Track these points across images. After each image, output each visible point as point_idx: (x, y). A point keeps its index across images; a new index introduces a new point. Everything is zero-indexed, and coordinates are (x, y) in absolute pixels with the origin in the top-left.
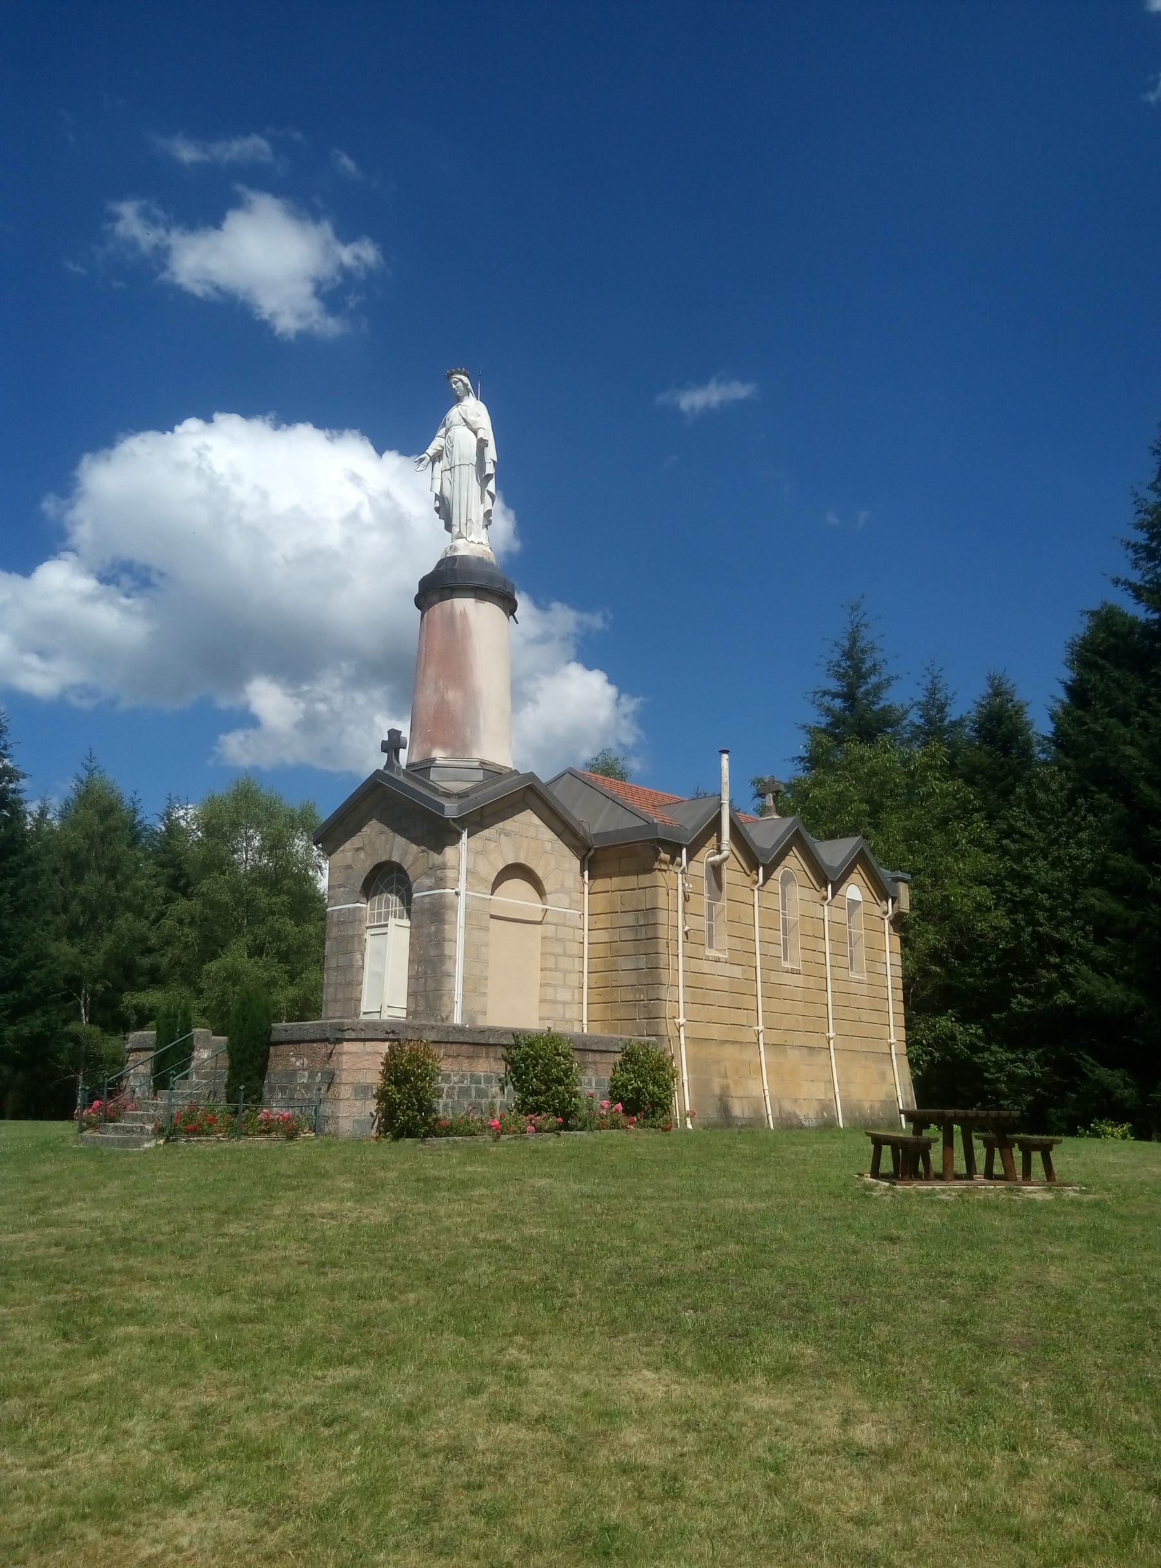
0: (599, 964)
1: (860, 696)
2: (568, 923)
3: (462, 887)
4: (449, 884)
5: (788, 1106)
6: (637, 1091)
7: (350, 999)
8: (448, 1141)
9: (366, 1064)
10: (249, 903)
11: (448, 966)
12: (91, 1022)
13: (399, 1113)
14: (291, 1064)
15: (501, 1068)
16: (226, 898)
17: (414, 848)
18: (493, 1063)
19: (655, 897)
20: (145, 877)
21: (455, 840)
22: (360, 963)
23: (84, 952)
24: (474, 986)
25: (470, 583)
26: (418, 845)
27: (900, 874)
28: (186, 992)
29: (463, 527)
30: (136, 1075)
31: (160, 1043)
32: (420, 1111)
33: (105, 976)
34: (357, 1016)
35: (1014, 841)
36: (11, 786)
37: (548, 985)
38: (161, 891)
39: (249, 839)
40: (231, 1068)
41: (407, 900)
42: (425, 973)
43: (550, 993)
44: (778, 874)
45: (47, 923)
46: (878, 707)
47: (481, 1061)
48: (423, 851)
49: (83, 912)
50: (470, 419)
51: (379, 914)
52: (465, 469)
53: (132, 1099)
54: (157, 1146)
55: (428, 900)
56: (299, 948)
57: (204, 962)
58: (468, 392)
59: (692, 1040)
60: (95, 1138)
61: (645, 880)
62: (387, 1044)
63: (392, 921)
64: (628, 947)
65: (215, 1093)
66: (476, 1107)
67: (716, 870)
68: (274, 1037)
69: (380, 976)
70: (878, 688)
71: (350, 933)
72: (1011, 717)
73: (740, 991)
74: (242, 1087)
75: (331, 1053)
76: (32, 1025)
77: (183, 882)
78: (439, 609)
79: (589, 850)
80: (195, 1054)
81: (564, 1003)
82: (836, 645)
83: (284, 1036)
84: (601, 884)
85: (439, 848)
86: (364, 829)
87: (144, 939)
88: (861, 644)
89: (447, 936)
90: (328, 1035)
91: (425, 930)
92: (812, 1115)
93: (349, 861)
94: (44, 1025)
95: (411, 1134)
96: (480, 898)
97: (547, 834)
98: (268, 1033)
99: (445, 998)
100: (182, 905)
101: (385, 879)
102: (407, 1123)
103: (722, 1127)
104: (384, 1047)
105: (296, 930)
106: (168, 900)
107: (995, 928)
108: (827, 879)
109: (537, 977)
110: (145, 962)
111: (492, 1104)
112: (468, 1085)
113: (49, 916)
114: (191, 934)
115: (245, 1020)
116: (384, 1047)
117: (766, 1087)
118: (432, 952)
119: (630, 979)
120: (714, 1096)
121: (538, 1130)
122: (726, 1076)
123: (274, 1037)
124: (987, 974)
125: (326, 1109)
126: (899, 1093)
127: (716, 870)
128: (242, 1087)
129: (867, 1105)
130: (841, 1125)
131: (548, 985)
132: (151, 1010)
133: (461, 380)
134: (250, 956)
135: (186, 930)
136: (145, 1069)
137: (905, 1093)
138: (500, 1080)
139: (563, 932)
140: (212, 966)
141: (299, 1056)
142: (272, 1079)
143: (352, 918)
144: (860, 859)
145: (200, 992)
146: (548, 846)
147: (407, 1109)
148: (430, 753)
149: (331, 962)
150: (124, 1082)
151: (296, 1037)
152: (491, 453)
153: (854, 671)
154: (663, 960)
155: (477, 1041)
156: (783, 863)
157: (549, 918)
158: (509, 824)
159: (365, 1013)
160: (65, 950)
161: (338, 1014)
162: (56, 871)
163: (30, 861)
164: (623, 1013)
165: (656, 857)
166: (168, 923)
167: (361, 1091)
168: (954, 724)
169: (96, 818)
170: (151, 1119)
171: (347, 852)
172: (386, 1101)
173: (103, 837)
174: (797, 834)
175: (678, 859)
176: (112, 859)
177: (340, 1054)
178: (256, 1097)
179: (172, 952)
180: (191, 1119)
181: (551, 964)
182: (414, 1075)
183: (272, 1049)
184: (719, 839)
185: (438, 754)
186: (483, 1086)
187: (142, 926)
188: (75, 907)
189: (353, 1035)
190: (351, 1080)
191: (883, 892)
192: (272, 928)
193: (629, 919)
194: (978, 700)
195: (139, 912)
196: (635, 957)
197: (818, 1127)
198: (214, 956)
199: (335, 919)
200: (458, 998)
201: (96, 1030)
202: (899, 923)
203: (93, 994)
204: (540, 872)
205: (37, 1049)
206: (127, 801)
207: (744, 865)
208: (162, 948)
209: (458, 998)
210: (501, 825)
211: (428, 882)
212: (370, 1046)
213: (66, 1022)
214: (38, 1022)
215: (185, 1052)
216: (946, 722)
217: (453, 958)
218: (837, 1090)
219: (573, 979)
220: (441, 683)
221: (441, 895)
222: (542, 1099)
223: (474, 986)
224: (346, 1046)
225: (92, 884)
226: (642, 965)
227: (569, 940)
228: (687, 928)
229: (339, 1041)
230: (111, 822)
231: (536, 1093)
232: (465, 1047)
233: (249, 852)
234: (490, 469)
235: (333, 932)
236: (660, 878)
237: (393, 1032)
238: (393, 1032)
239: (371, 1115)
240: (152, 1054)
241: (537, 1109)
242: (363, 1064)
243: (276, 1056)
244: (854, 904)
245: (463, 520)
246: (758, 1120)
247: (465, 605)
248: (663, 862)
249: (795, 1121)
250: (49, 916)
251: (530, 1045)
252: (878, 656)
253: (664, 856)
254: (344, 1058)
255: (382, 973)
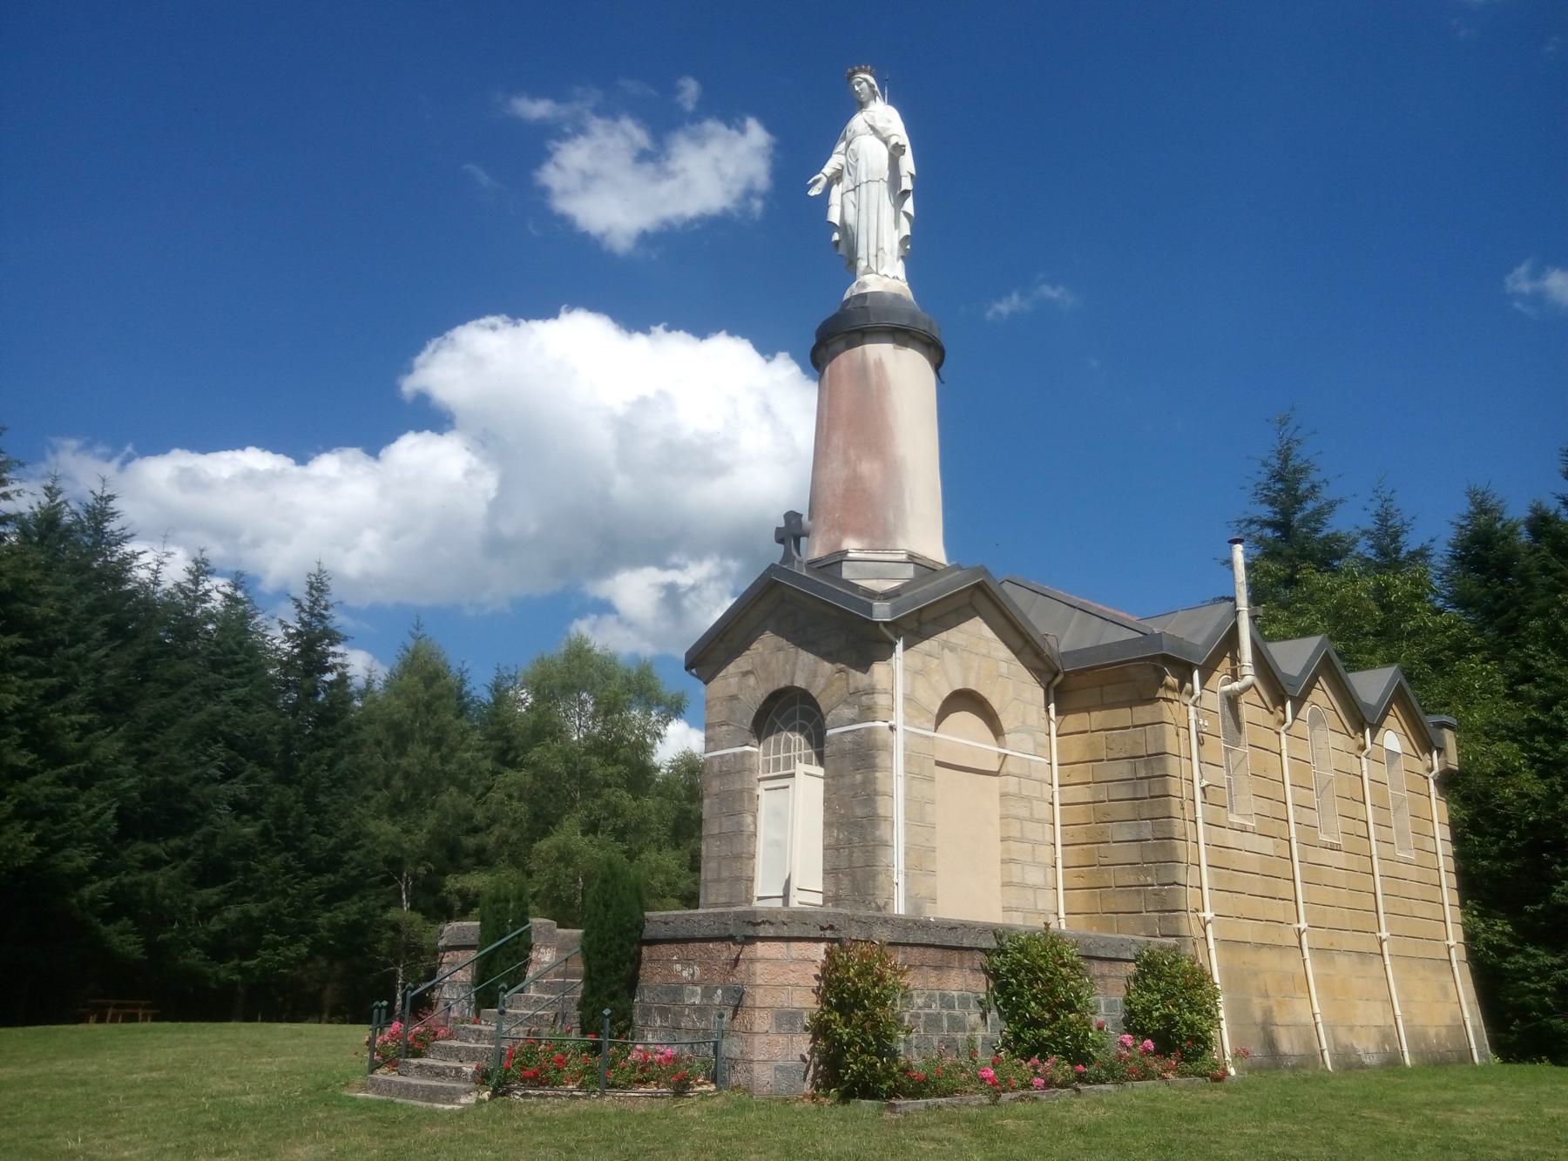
0: (1079, 834)
1: (1295, 524)
2: (1035, 775)
3: (898, 719)
4: (879, 715)
5: (1345, 1038)
6: (1168, 1018)
7: (738, 879)
8: (928, 1107)
9: (792, 978)
10: (584, 772)
11: (882, 831)
12: (412, 908)
13: (849, 1058)
14: (669, 970)
15: (980, 985)
16: (559, 767)
17: (827, 667)
18: (970, 978)
19: (1161, 738)
20: (472, 752)
21: (886, 652)
22: (752, 828)
23: (407, 831)
24: (920, 860)
25: (886, 323)
26: (832, 662)
27: (1445, 718)
28: (515, 874)
29: (872, 260)
30: (452, 984)
31: (485, 939)
32: (880, 1055)
33: (427, 858)
34: (749, 901)
35: (1538, 686)
36: (332, 649)
37: (1011, 861)
38: (488, 764)
39: (583, 703)
40: (588, 978)
41: (817, 740)
42: (850, 841)
43: (1016, 872)
44: (1306, 711)
45: (367, 799)
46: (1320, 535)
47: (953, 973)
48: (841, 671)
49: (406, 788)
50: (879, 125)
51: (777, 761)
52: (874, 186)
53: (446, 1019)
54: (480, 1102)
55: (849, 737)
56: (637, 826)
57: (534, 841)
58: (874, 94)
59: (1224, 943)
60: (390, 1082)
61: (1143, 713)
62: (823, 946)
63: (801, 768)
64: (1124, 810)
65: (561, 1016)
66: (950, 1044)
67: (1232, 701)
68: (650, 931)
69: (779, 845)
70: (1318, 515)
71: (738, 786)
72: (1505, 538)
73: (1275, 872)
74: (607, 1012)
75: (737, 960)
76: (348, 911)
77: (511, 755)
78: (845, 361)
79: (1056, 675)
80: (534, 955)
81: (1035, 888)
82: (1265, 464)
83: (663, 931)
84: (1074, 721)
85: (864, 665)
86: (754, 646)
87: (469, 817)
88: (1295, 462)
89: (880, 787)
90: (732, 931)
91: (847, 781)
92: (1372, 1049)
93: (733, 690)
94: (360, 911)
95: (868, 1093)
96: (921, 736)
97: (1003, 652)
98: (640, 926)
99: (881, 878)
100: (511, 775)
101: (787, 711)
102: (861, 1074)
103: (1268, 1069)
104: (819, 951)
105: (634, 804)
106: (494, 773)
107: (1522, 795)
108: (1362, 720)
109: (997, 849)
110: (470, 842)
111: (971, 1041)
112: (941, 1010)
113: (369, 791)
114: (521, 809)
115: (607, 906)
116: (819, 951)
117: (1317, 1010)
118: (859, 812)
119: (1132, 853)
120: (1256, 1024)
121: (1049, 1084)
122: (1267, 996)
123: (650, 931)
124: (1505, 855)
125: (732, 1048)
126: (1467, 1015)
127: (1232, 701)
128: (607, 1012)
129: (1432, 1032)
130: (1408, 1061)
131: (1011, 861)
132: (477, 895)
133: (864, 81)
134: (584, 834)
135: (515, 804)
136: (464, 976)
137: (1471, 1015)
138: (981, 1003)
139: (1029, 788)
140: (543, 845)
141: (686, 962)
142: (646, 996)
143: (739, 767)
144: (1398, 697)
145: (529, 874)
146: (1004, 667)
147: (855, 1053)
148: (839, 544)
149: (711, 827)
150: (436, 994)
151: (682, 933)
152: (908, 164)
153: (1287, 490)
154: (1178, 827)
155: (947, 944)
156: (1310, 698)
157: (1010, 766)
158: (954, 635)
159: (760, 899)
160: (385, 829)
161: (722, 900)
162: (379, 743)
163: (349, 729)
164: (1120, 903)
165: (1160, 682)
166: (496, 795)
167: (785, 1019)
168: (1413, 556)
169: (421, 686)
170: (472, 1055)
171: (730, 678)
172: (826, 1038)
173: (428, 706)
174: (1327, 660)
175: (1188, 685)
176: (437, 730)
177: (752, 961)
178: (624, 1025)
179: (497, 830)
180: (530, 1060)
181: (1015, 831)
182: (867, 996)
183: (645, 950)
184: (1235, 660)
185: (851, 545)
186: (957, 1012)
187: (467, 802)
188: (397, 782)
189: (771, 932)
190: (768, 1002)
191: (1426, 742)
192: (608, 803)
193: (1122, 770)
194: (1456, 520)
195: (464, 787)
196: (1134, 821)
197: (1382, 1066)
198: (545, 833)
199: (716, 768)
200: (899, 878)
201: (418, 917)
202: (1448, 782)
203: (415, 878)
204: (995, 702)
205: (354, 940)
206: (454, 670)
207: (1266, 699)
208: (489, 826)
209: (899, 878)
210: (944, 635)
211: (848, 712)
212: (797, 949)
213: (385, 908)
214: (355, 908)
215: (519, 952)
216: (1403, 554)
217: (889, 819)
218: (1398, 1012)
219: (1044, 853)
220: (852, 453)
221: (870, 731)
222: (1046, 1033)
223: (920, 860)
224: (761, 949)
225: (416, 756)
226: (1146, 832)
227: (1038, 799)
228: (1205, 783)
229: (750, 940)
230: (436, 689)
231: (1036, 1024)
232: (931, 951)
233: (579, 725)
234: (907, 184)
235: (715, 786)
236: (1169, 711)
237: (831, 927)
238: (831, 927)
239: (803, 1059)
240: (473, 954)
241: (1039, 1049)
242: (787, 978)
243: (651, 960)
244: (1393, 755)
245: (873, 251)
246: (1311, 1058)
247: (880, 352)
248: (1169, 688)
249: (1354, 1059)
250: (369, 791)
251: (1021, 950)
252: (1315, 477)
253: (1171, 680)
254: (759, 967)
255: (785, 839)
